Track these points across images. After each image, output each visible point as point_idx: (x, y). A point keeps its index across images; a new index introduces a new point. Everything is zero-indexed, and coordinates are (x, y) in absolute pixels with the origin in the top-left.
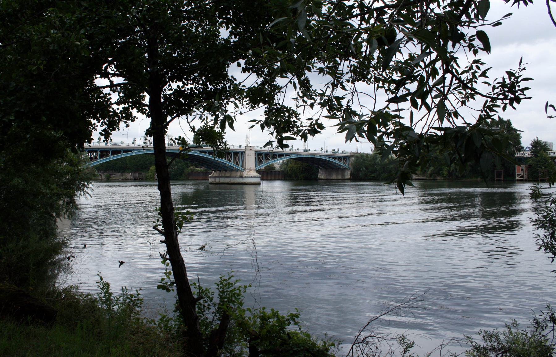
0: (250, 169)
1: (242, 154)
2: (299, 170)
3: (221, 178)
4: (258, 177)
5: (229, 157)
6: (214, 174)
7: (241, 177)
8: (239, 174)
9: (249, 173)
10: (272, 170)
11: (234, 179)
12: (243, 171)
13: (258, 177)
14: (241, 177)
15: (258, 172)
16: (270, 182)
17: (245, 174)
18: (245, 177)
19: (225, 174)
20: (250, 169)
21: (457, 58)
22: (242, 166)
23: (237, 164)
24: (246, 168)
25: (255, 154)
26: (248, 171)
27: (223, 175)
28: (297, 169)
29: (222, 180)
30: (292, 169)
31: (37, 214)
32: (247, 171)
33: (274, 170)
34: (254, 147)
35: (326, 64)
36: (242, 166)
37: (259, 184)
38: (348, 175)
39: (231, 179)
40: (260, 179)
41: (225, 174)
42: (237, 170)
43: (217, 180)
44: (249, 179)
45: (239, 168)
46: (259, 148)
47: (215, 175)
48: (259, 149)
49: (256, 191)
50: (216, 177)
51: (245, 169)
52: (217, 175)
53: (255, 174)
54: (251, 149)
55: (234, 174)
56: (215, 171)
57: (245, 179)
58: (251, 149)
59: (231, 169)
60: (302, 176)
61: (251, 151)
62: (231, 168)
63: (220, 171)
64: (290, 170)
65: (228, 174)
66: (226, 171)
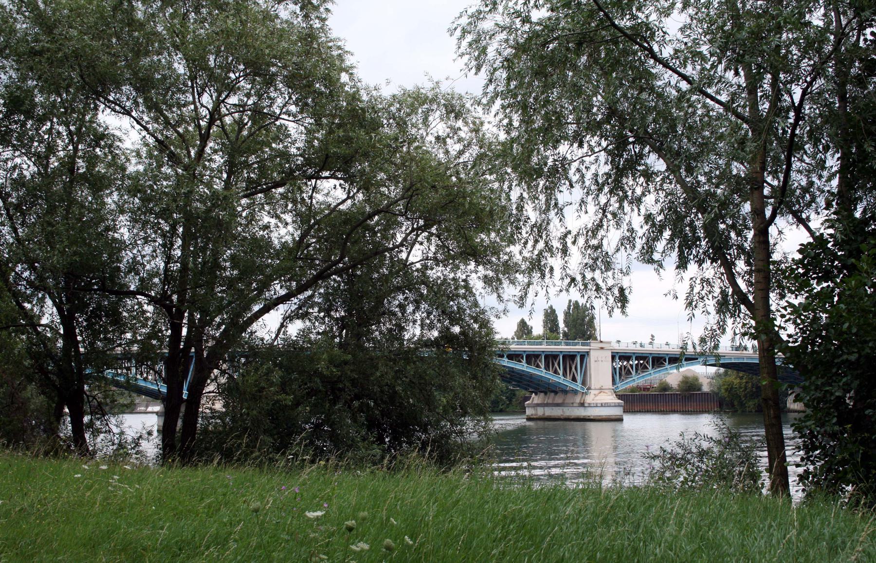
0: (601, 389)
1: (583, 357)
2: (746, 389)
3: (546, 409)
4: (619, 405)
5: (556, 365)
6: (536, 399)
7: (582, 405)
8: (578, 399)
9: (597, 398)
10: (694, 390)
11: (570, 409)
12: (586, 394)
13: (619, 405)
14: (582, 405)
15: (620, 397)
16: (689, 416)
17: (589, 399)
18: (590, 406)
19: (554, 399)
20: (601, 389)
21: (352, 67)
22: (584, 383)
23: (574, 379)
24: (593, 387)
25: (613, 358)
26: (597, 392)
27: (550, 401)
28: (741, 388)
29: (549, 412)
30: (730, 389)
31: (427, 514)
32: (593, 392)
33: (700, 389)
34: (610, 343)
35: (101, 42)
36: (584, 383)
37: (620, 420)
38: (55, 423)
39: (565, 409)
40: (621, 409)
41: (554, 399)
42: (575, 392)
43: (540, 412)
44: (597, 409)
45: (578, 386)
46: (638, 345)
47: (536, 402)
48: (638, 348)
49: (615, 436)
50: (538, 405)
51: (589, 389)
52: (539, 402)
53: (612, 399)
54: (602, 348)
55: (569, 399)
56: (536, 394)
57: (589, 409)
58: (602, 348)
59: (565, 391)
60: (751, 403)
61: (602, 351)
62: (564, 388)
63: (546, 393)
64: (726, 390)
65: (559, 399)
66: (556, 393)
